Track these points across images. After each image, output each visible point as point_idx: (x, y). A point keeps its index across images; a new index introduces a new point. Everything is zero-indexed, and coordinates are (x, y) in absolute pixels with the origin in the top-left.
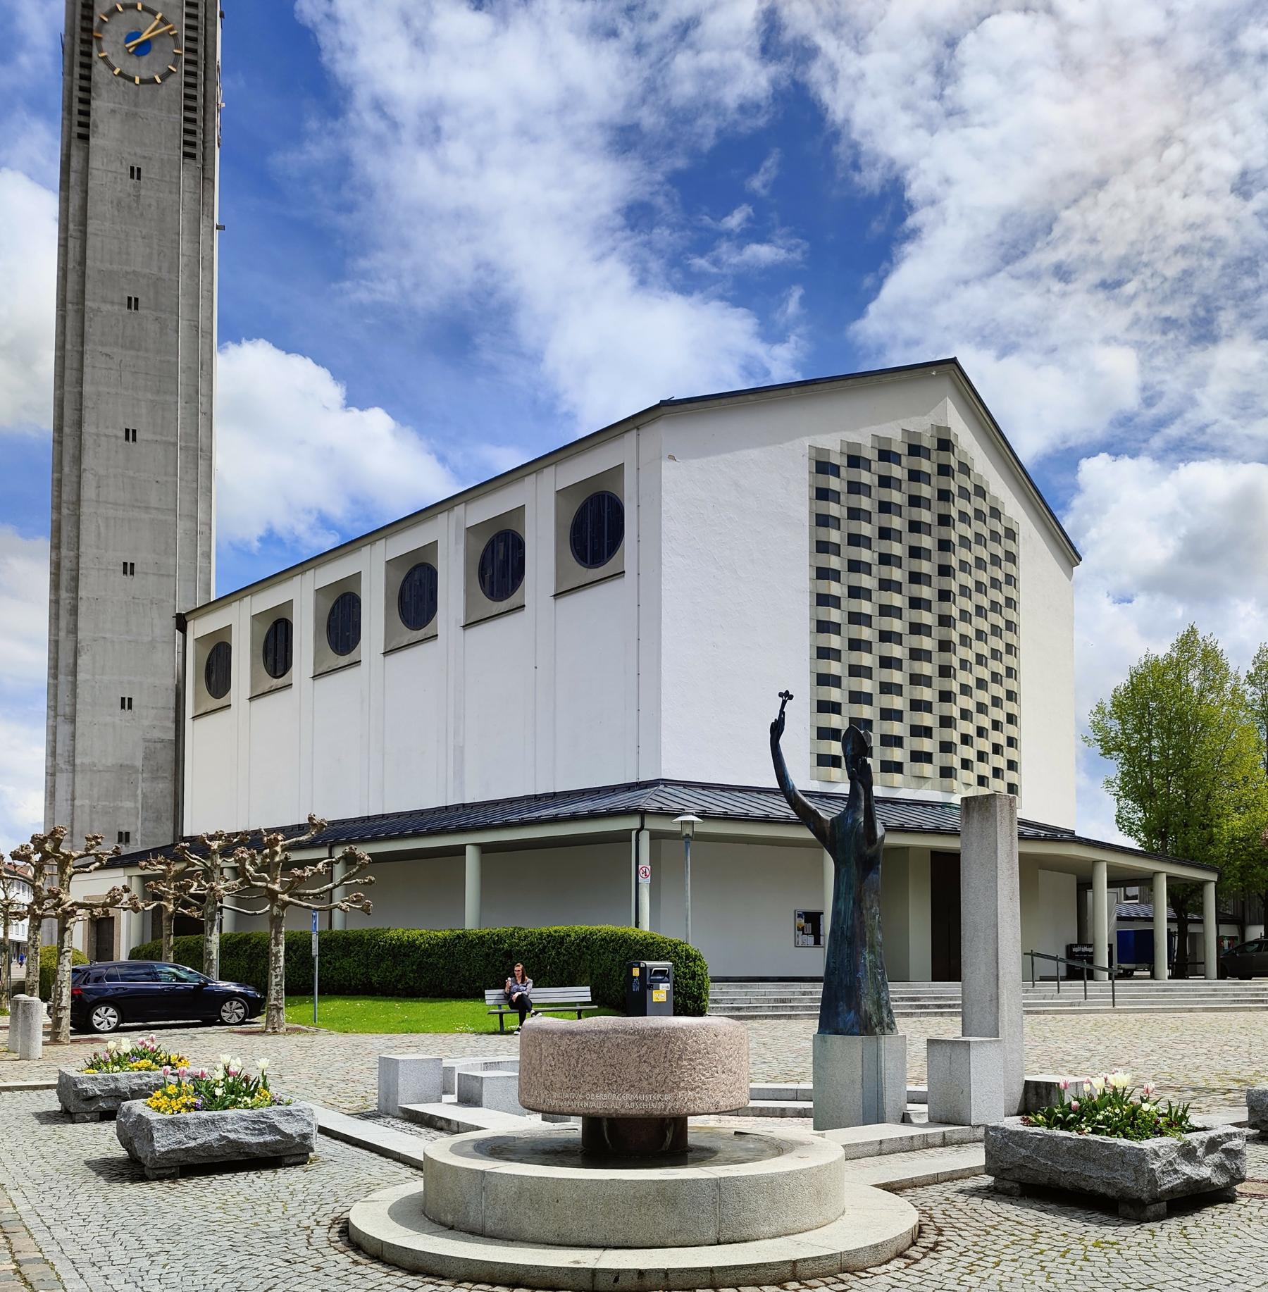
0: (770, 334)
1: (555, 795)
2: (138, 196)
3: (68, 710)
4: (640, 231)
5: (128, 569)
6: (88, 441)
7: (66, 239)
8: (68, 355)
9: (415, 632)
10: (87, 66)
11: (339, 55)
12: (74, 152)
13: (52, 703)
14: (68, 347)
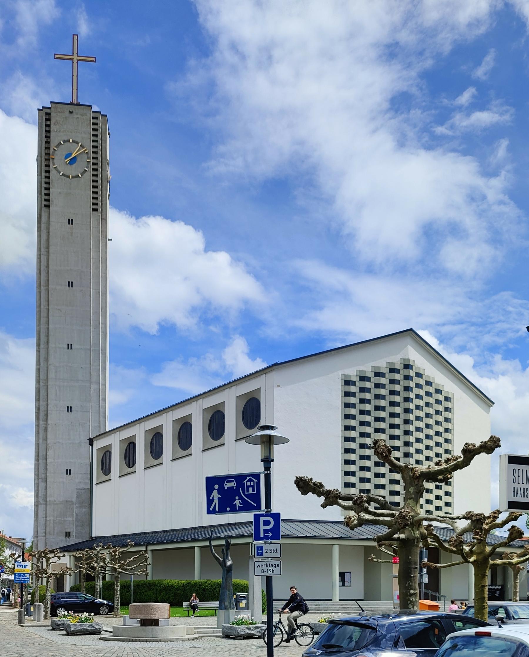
0: (488, 172)
1: (235, 524)
2: (72, 233)
3: (43, 476)
4: (402, 113)
5: (69, 409)
6: (51, 351)
7: (40, 255)
8: (42, 311)
9: (184, 451)
10: (48, 172)
11: (209, 17)
12: (43, 213)
13: (36, 473)
14: (42, 307)
